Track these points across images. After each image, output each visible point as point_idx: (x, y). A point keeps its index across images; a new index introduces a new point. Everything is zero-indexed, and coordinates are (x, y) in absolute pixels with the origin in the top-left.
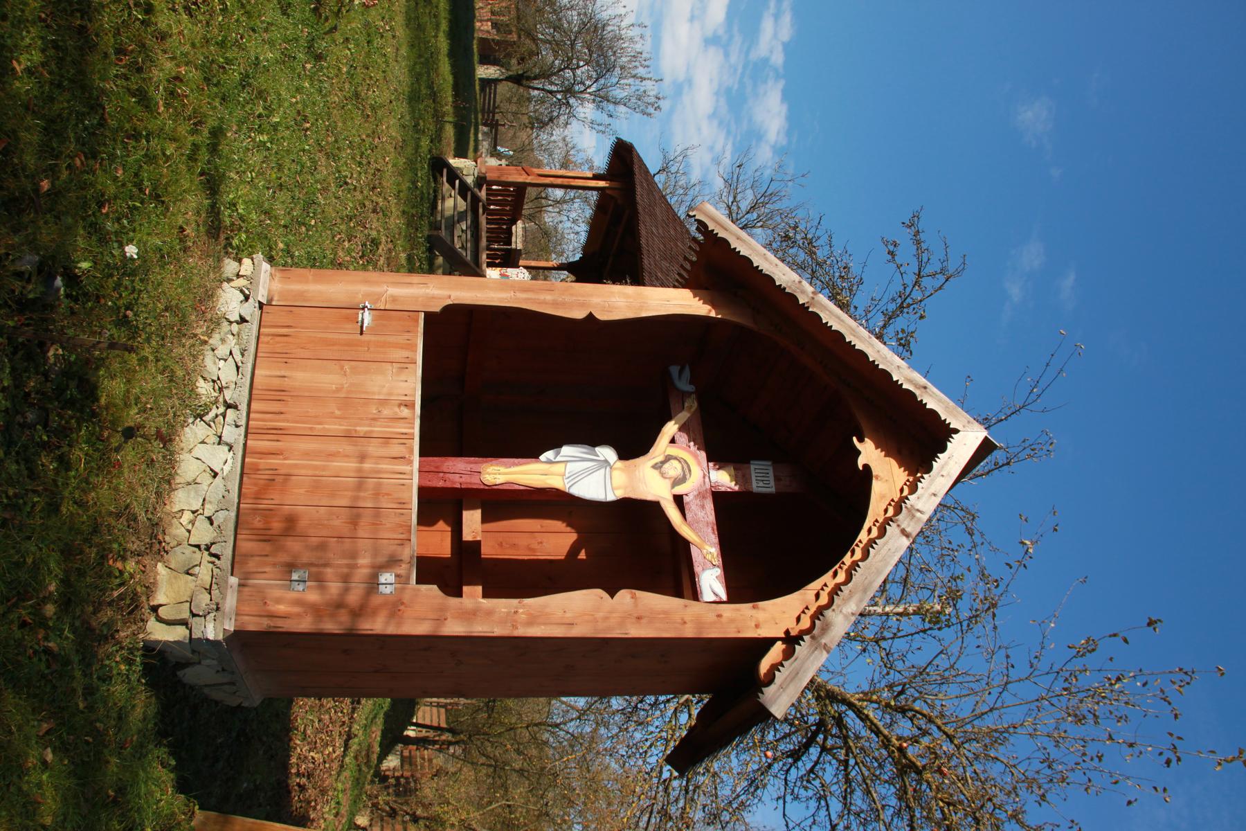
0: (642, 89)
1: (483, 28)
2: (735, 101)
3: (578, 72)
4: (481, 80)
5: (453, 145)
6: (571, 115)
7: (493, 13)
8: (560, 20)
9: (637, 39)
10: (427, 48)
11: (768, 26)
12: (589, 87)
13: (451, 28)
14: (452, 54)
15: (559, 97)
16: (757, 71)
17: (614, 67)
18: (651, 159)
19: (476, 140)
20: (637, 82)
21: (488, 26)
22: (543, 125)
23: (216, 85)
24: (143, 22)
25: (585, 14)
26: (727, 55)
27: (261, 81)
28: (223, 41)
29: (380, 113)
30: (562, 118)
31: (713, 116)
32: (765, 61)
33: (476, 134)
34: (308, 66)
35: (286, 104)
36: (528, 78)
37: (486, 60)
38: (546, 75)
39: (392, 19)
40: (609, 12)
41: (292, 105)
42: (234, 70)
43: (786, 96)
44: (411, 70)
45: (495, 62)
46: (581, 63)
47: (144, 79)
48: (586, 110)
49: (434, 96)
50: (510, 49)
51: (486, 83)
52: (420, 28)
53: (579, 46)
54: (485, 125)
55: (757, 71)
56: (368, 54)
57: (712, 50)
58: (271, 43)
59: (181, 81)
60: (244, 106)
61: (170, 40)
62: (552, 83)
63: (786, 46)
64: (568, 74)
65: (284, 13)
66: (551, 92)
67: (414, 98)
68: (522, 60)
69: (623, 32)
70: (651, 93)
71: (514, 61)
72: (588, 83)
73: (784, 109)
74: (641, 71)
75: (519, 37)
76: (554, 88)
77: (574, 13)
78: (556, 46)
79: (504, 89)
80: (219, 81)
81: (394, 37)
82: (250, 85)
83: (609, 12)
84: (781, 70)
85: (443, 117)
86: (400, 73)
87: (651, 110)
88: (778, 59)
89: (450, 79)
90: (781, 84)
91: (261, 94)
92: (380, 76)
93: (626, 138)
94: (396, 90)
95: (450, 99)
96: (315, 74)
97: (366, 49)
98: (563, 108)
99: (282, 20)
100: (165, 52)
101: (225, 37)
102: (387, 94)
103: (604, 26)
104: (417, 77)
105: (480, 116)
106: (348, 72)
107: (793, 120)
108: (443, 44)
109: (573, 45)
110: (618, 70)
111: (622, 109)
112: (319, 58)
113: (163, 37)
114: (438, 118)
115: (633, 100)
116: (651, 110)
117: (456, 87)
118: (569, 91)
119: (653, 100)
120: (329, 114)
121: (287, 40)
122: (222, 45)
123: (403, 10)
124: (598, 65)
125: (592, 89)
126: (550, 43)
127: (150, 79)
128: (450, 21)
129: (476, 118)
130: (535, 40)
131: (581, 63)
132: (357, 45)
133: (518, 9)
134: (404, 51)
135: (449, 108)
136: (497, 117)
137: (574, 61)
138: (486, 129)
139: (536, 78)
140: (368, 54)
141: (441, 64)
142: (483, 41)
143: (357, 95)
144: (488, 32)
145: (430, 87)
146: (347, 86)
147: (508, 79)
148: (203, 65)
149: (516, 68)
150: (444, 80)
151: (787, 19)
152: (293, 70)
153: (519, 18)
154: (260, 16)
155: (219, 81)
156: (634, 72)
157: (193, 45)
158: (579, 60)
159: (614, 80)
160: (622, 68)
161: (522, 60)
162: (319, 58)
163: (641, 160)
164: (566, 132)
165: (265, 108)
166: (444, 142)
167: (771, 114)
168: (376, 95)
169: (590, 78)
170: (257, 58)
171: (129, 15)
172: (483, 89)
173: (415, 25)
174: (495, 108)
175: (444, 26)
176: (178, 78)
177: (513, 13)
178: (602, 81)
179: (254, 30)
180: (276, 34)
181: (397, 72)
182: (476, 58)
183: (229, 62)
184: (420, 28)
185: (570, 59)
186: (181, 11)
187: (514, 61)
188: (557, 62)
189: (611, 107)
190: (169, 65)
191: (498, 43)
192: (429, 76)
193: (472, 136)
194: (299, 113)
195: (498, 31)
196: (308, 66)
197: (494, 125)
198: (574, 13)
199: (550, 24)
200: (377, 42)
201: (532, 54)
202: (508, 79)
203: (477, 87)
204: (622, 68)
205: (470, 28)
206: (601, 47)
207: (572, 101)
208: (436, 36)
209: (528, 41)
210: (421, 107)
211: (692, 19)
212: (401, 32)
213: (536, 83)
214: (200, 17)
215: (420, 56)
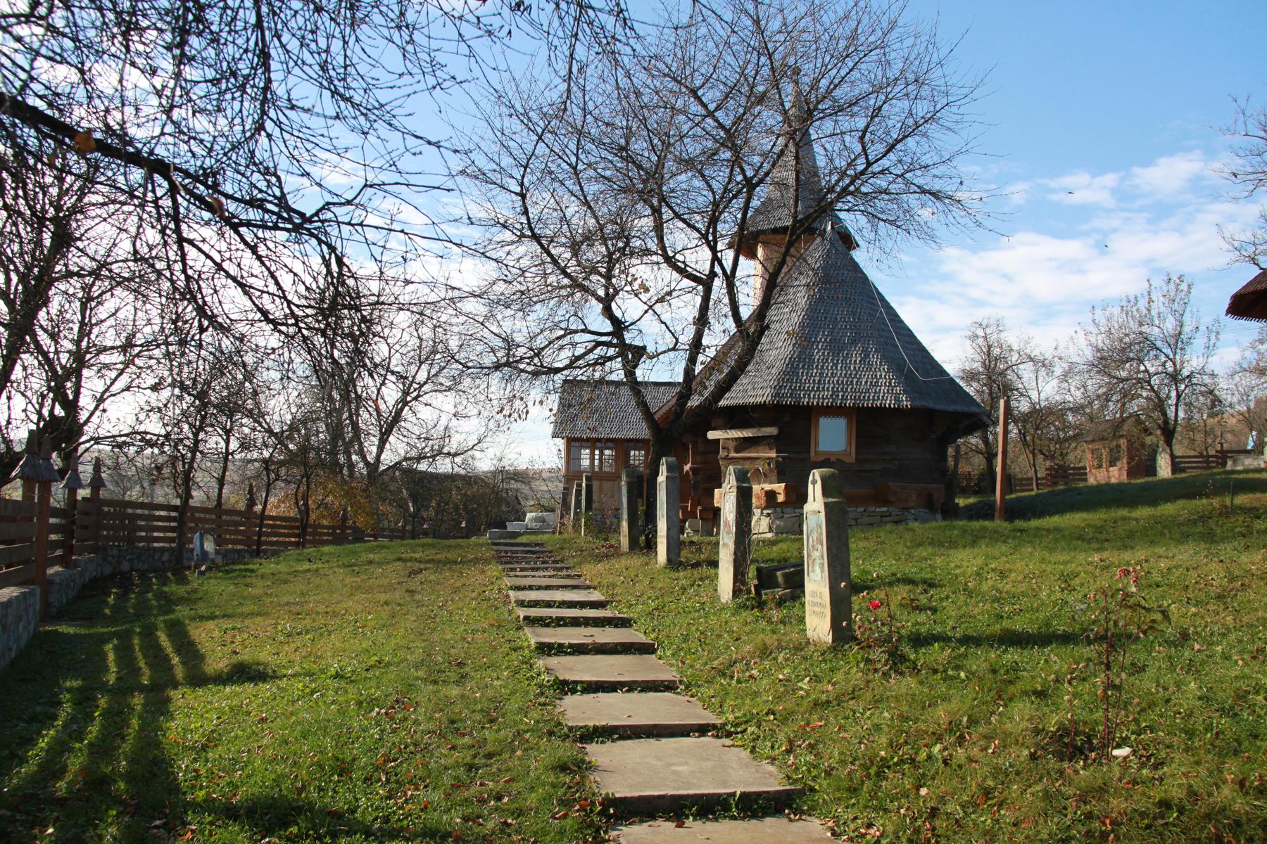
0: (1162, 299)
1: (1116, 474)
2: (1161, 212)
3: (1152, 370)
4: (1174, 471)
5: (1258, 495)
6: (1202, 372)
7: (1100, 467)
8: (1098, 397)
9: (1107, 313)
10: (1152, 528)
11: (1078, 197)
12: (1167, 356)
13: (1125, 506)
14: (1153, 502)
15: (1183, 387)
16: (1125, 197)
17: (1141, 333)
18: (1246, 275)
19: (1246, 471)
20: (1154, 306)
21: (1114, 471)
22: (1216, 401)
23: (1240, 744)
24: (1181, 812)
25: (1089, 371)
26: (1114, 231)
27: (1225, 695)
28: (1186, 733)
29: (1237, 573)
30: (1207, 380)
31: (1181, 231)
32: (1114, 191)
33: (1239, 472)
34: (1197, 647)
35: (1246, 670)
36: (1166, 421)
37: (1151, 469)
38: (1160, 405)
39: (1128, 564)
40: (1084, 347)
41: (1246, 664)
42: (1218, 723)
43: (1147, 163)
44: (1180, 542)
45: (1153, 460)
46: (1142, 368)
47: (1249, 820)
48: (1192, 361)
49: (1204, 518)
50: (1136, 445)
51: (1176, 466)
52: (1131, 535)
53: (1124, 374)
54: (1224, 464)
55: (1125, 197)
56: (1171, 586)
57: (1112, 246)
58: (1178, 685)
59: (1244, 779)
60: (1259, 716)
61: (1195, 788)
62: (1168, 397)
63: (1094, 176)
64: (1155, 381)
65: (1143, 669)
66: (1178, 396)
67: (1209, 537)
68: (1146, 431)
69: (1103, 330)
70: (1165, 289)
71: (1148, 440)
72: (1163, 358)
73: (1163, 161)
74: (1142, 304)
75: (1121, 436)
76: (1173, 394)
77: (1089, 382)
78: (1127, 396)
79: (1179, 450)
80: (1236, 740)
81: (1147, 561)
82: (1232, 708)
83: (1084, 347)
84: (1121, 174)
85: (1226, 507)
86: (1185, 554)
87: (1184, 287)
88: (1110, 179)
89: (1180, 503)
90: (1137, 170)
91: (1241, 696)
92: (1193, 574)
93: (1226, 303)
94: (1206, 557)
95: (1204, 501)
96: (1204, 640)
97: (1165, 588)
98: (1194, 380)
99: (1151, 672)
100: (1210, 794)
101: (1182, 730)
102: (1214, 565)
103: (1098, 350)
104: (1185, 537)
105: (1216, 470)
106: (1196, 606)
107: (1172, 149)
108: (1143, 512)
109: (1123, 380)
110: (1144, 329)
111: (1187, 318)
112: (1185, 636)
113: (1193, 794)
114: (1228, 512)
115: (1175, 307)
116: (1184, 287)
117: (1190, 496)
118: (1175, 377)
119: (1172, 286)
120: (1251, 626)
121: (1172, 668)
122: (1191, 734)
123: (1116, 553)
124: (1141, 350)
125: (1168, 351)
126: (1124, 405)
127: (1247, 813)
128: (1118, 507)
129: (1219, 474)
130: (1123, 420)
131: (1142, 368)
132: (1163, 597)
133: (1093, 441)
134: (1160, 550)
135: (1216, 502)
136: (1212, 452)
137: (1141, 376)
138: (1230, 463)
139: (1164, 414)
140: (1171, 586)
141: (1166, 513)
142: (1131, 473)
143: (1220, 597)
144: (1120, 469)
145: (1195, 522)
146: (1211, 607)
147: (1169, 443)
148: (1219, 755)
149: (1156, 438)
150: (1183, 509)
151: (1068, 181)
152: (1203, 663)
153: (1102, 439)
154: (1152, 694)
155: (1236, 740)
156: (1145, 312)
157: (1198, 763)
158: (1139, 372)
159: (1156, 330)
160: (1141, 324)
161: (1146, 431)
162: (1185, 636)
163: (1250, 283)
164: (1221, 374)
165: (1257, 693)
166: (1257, 505)
167: (1169, 174)
168: (1216, 575)
169: (1156, 357)
170: (1200, 698)
171: (1174, 826)
172: (1183, 470)
173: (1128, 540)
174: (1201, 455)
175: (1123, 512)
176: (1242, 784)
177: (1097, 446)
178: (1159, 344)
179: (1168, 701)
180: (1168, 679)
181: (1185, 557)
182: (1150, 479)
183: (1208, 728)
184: (1131, 535)
185: (1139, 381)
186: (1160, 772)
187: (1148, 440)
188: (1145, 394)
189: (1187, 329)
190: (1226, 791)
191: (1131, 458)
192: (1182, 524)
193: (1242, 476)
194: (1254, 658)
195: (1118, 459)
196: (1197, 647)
197: (1223, 456)
198: (1089, 382)
199: (1104, 407)
200: (1156, 577)
201: (1138, 421)
202: (1169, 443)
203: (1183, 475)
204: (1141, 324)
205: (1119, 488)
206: (1123, 350)
207: (1185, 372)
208: (1136, 519)
209: (1126, 427)
210: (1218, 531)
211: (1081, 271)
212: (1141, 554)
213: (1171, 413)
214: (1163, 754)
215: (1162, 534)
